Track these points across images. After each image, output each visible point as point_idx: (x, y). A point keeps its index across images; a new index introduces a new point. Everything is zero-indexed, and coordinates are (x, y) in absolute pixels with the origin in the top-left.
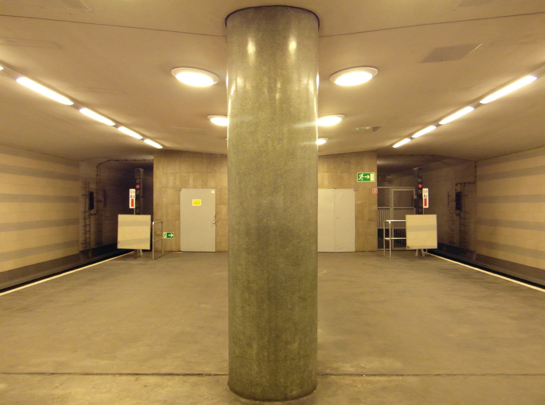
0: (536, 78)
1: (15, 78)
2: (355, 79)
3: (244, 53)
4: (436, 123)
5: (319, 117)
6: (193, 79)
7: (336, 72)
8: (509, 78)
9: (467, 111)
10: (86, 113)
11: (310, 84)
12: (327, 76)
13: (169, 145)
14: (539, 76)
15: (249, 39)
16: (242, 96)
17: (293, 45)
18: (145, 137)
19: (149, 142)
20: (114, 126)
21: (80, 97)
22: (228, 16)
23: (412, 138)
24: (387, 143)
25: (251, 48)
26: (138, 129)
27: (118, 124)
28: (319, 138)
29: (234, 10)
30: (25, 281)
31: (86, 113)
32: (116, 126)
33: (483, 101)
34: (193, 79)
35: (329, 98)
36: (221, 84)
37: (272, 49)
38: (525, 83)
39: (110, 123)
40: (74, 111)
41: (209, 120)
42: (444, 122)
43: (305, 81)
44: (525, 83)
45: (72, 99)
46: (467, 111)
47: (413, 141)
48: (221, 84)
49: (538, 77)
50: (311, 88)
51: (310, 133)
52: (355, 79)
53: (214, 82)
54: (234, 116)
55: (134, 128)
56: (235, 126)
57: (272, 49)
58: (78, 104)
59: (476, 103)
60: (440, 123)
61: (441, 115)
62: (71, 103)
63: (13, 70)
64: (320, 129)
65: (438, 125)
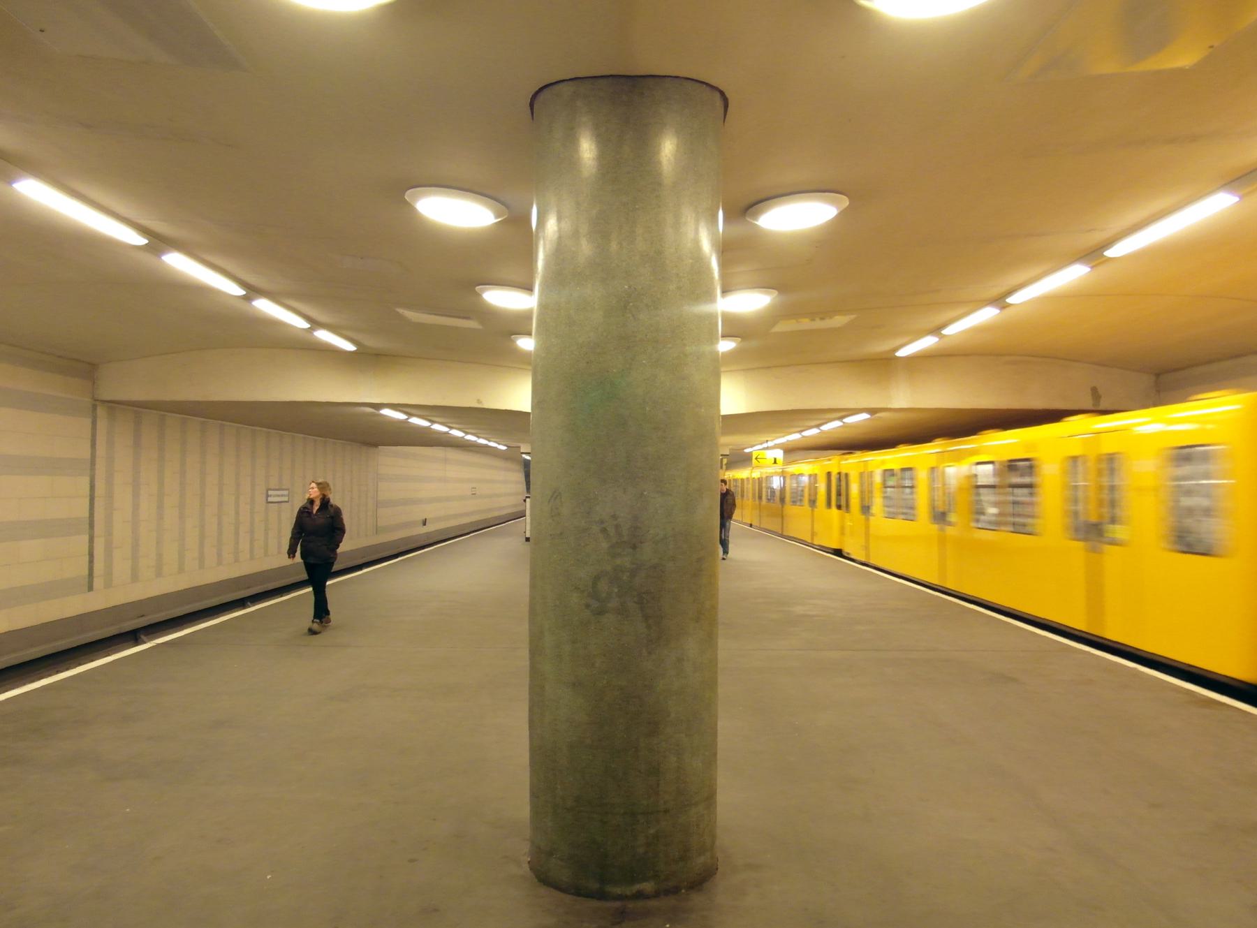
0: (1237, 199)
2: (797, 218)
3: (572, 162)
4: (999, 300)
6: (454, 213)
10: (178, 263)
11: (703, 237)
13: (371, 342)
16: (560, 253)
17: (668, 148)
18: (315, 324)
19: (324, 336)
23: (1004, 306)
25: (587, 149)
27: (253, 291)
28: (723, 336)
31: (178, 263)
32: (311, 329)
33: (1109, 253)
34: (454, 213)
35: (745, 256)
37: (627, 190)
39: (300, 323)
40: (147, 258)
41: (479, 295)
43: (689, 230)
44: (1216, 206)
48: (516, 228)
50: (706, 246)
52: (797, 218)
55: (345, 332)
56: (543, 306)
57: (627, 190)
58: (159, 243)
62: (241, 292)
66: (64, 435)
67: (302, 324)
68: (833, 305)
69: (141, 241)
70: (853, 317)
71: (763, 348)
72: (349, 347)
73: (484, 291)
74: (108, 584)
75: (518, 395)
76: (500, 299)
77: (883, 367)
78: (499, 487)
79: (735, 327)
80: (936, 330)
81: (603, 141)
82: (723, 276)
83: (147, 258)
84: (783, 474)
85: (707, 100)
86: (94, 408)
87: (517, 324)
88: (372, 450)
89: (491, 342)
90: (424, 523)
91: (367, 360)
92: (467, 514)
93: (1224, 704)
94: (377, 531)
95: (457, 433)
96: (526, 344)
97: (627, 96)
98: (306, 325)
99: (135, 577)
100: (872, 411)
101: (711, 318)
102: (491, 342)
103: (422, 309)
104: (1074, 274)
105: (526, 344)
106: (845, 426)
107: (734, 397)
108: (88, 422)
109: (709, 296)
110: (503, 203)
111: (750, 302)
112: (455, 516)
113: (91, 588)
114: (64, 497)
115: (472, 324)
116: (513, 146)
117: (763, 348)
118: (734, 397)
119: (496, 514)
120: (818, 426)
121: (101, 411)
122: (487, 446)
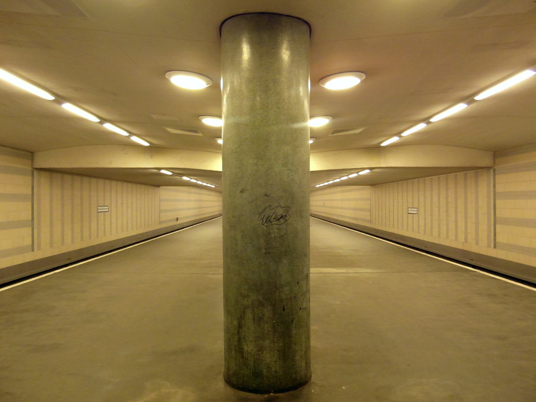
2: (343, 83)
4: (426, 120)
5: (311, 117)
6: (187, 83)
7: (329, 76)
8: (510, 72)
9: (460, 108)
10: (69, 108)
12: (319, 79)
13: (155, 142)
15: (244, 40)
17: (285, 55)
18: (131, 134)
19: (135, 139)
21: (61, 92)
23: (429, 123)
24: (375, 142)
25: (246, 51)
26: (123, 126)
27: (103, 120)
29: (230, 16)
30: (55, 267)
31: (69, 108)
32: (101, 123)
33: (477, 98)
34: (187, 83)
36: (215, 87)
37: (265, 53)
38: (523, 77)
39: (94, 119)
40: (100, 125)
41: (200, 121)
42: (405, 134)
44: (523, 77)
45: (98, 117)
46: (421, 127)
47: (402, 139)
48: (215, 87)
52: (343, 83)
53: (207, 85)
54: (227, 118)
55: (144, 138)
56: (226, 125)
57: (265, 53)
58: (60, 99)
59: (427, 121)
60: (431, 120)
61: (474, 90)
62: (98, 120)
64: (312, 131)
65: (429, 123)
66: (16, 183)
67: (125, 134)
68: (356, 126)
69: (52, 98)
70: (365, 128)
71: (325, 142)
72: (147, 144)
73: (202, 119)
74: (39, 249)
75: (216, 164)
76: (209, 122)
77: (377, 150)
78: (212, 203)
79: (315, 135)
80: (398, 134)
81: (253, 45)
82: (310, 111)
83: (56, 106)
84: (275, 237)
85: (302, 25)
86: (33, 172)
87: (215, 133)
88: (157, 189)
89: (206, 141)
90: (177, 219)
91: (153, 150)
92: (214, 212)
93: (500, 280)
94: (160, 223)
95: (193, 181)
96: (220, 141)
97: (266, 25)
98: (127, 134)
99: (73, 242)
100: (371, 169)
101: (304, 129)
102: (206, 141)
103: (178, 127)
104: (460, 108)
105: (220, 141)
106: (359, 175)
107: (315, 164)
108: (31, 178)
109: (304, 120)
110: (210, 79)
111: (319, 123)
112: (211, 213)
113: (33, 250)
114: (23, 211)
115: (201, 135)
116: (214, 50)
117: (325, 142)
118: (315, 164)
119: (212, 214)
120: (347, 176)
121: (36, 173)
122: (206, 186)
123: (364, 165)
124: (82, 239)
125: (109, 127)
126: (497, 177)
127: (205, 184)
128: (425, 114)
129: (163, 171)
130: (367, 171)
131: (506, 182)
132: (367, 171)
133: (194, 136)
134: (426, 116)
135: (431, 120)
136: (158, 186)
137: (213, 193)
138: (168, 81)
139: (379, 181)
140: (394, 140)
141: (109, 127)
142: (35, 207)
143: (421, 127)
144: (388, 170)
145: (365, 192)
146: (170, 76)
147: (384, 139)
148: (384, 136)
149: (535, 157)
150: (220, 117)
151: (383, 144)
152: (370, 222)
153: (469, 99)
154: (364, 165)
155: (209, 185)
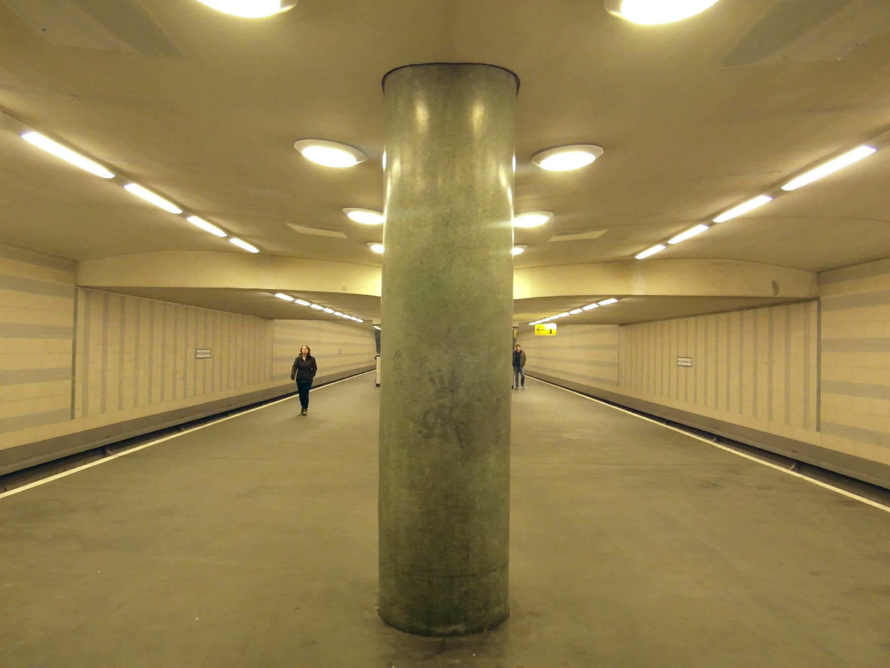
0: (874, 151)
1: (20, 132)
2: (568, 162)
4: (708, 220)
5: (517, 213)
6: (328, 157)
9: (760, 202)
10: (135, 191)
11: (502, 175)
12: (531, 154)
13: (270, 247)
14: (878, 147)
16: (402, 186)
17: (478, 114)
18: (231, 234)
19: (236, 242)
20: (181, 215)
22: (385, 77)
23: (712, 224)
24: (626, 252)
25: (422, 114)
27: (187, 211)
31: (135, 191)
33: (787, 187)
34: (328, 157)
38: (860, 155)
40: (114, 187)
42: (674, 241)
44: (860, 155)
46: (699, 230)
49: (773, 198)
50: (504, 181)
51: (504, 238)
52: (568, 162)
53: (358, 160)
54: (389, 215)
56: (389, 223)
58: (122, 176)
60: (715, 220)
62: (180, 211)
63: (19, 121)
65: (712, 224)
67: (221, 234)
68: (591, 227)
69: (110, 175)
71: (543, 252)
72: (255, 250)
75: (372, 284)
76: (359, 217)
77: (627, 266)
79: (524, 238)
80: (664, 241)
81: (432, 109)
82: (516, 202)
83: (114, 187)
85: (507, 80)
86: (76, 290)
87: (372, 235)
88: (270, 322)
89: (352, 248)
91: (266, 259)
94: (273, 378)
96: (378, 249)
97: (449, 77)
98: (224, 235)
100: (619, 297)
101: (507, 231)
103: (306, 222)
104: (760, 202)
105: (378, 249)
106: (600, 307)
107: (523, 287)
109: (505, 216)
111: (534, 221)
113: (73, 418)
114: (53, 354)
117: (543, 252)
118: (523, 287)
120: (581, 307)
121: (81, 294)
122: (349, 320)
123: (608, 291)
124: (136, 403)
125: (196, 222)
126: (823, 314)
127: (346, 316)
128: (664, 234)
129: (279, 296)
130: (613, 301)
131: (840, 323)
132: (613, 301)
133: (320, 237)
134: (775, 177)
135: (715, 220)
136: (272, 319)
137: (358, 332)
138: (299, 155)
139: (633, 317)
140: (657, 249)
141: (196, 222)
142: (80, 348)
143: (699, 230)
144: (639, 300)
145: (609, 335)
146: (302, 147)
147: (673, 230)
148: (642, 243)
149: (887, 282)
150: (380, 210)
151: (640, 257)
152: (618, 384)
153: (773, 188)
154: (608, 291)
155: (353, 318)
